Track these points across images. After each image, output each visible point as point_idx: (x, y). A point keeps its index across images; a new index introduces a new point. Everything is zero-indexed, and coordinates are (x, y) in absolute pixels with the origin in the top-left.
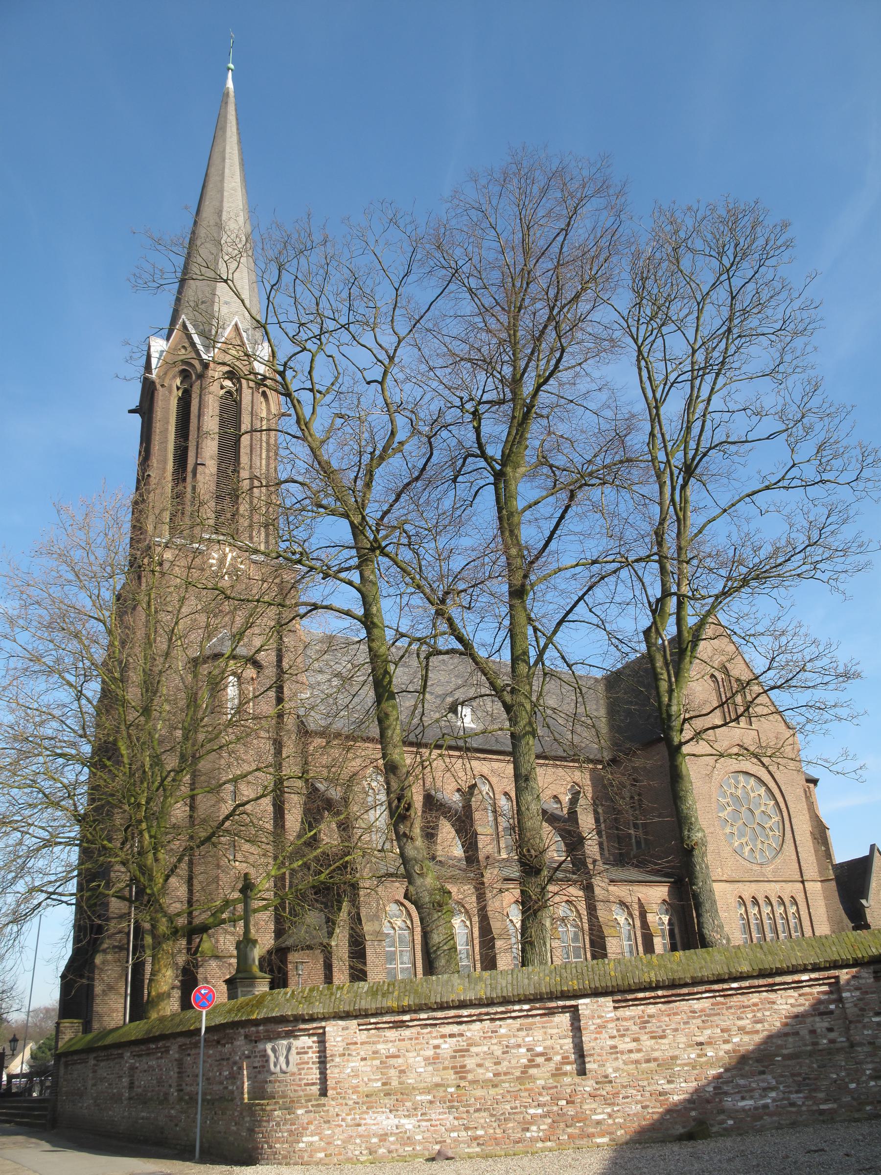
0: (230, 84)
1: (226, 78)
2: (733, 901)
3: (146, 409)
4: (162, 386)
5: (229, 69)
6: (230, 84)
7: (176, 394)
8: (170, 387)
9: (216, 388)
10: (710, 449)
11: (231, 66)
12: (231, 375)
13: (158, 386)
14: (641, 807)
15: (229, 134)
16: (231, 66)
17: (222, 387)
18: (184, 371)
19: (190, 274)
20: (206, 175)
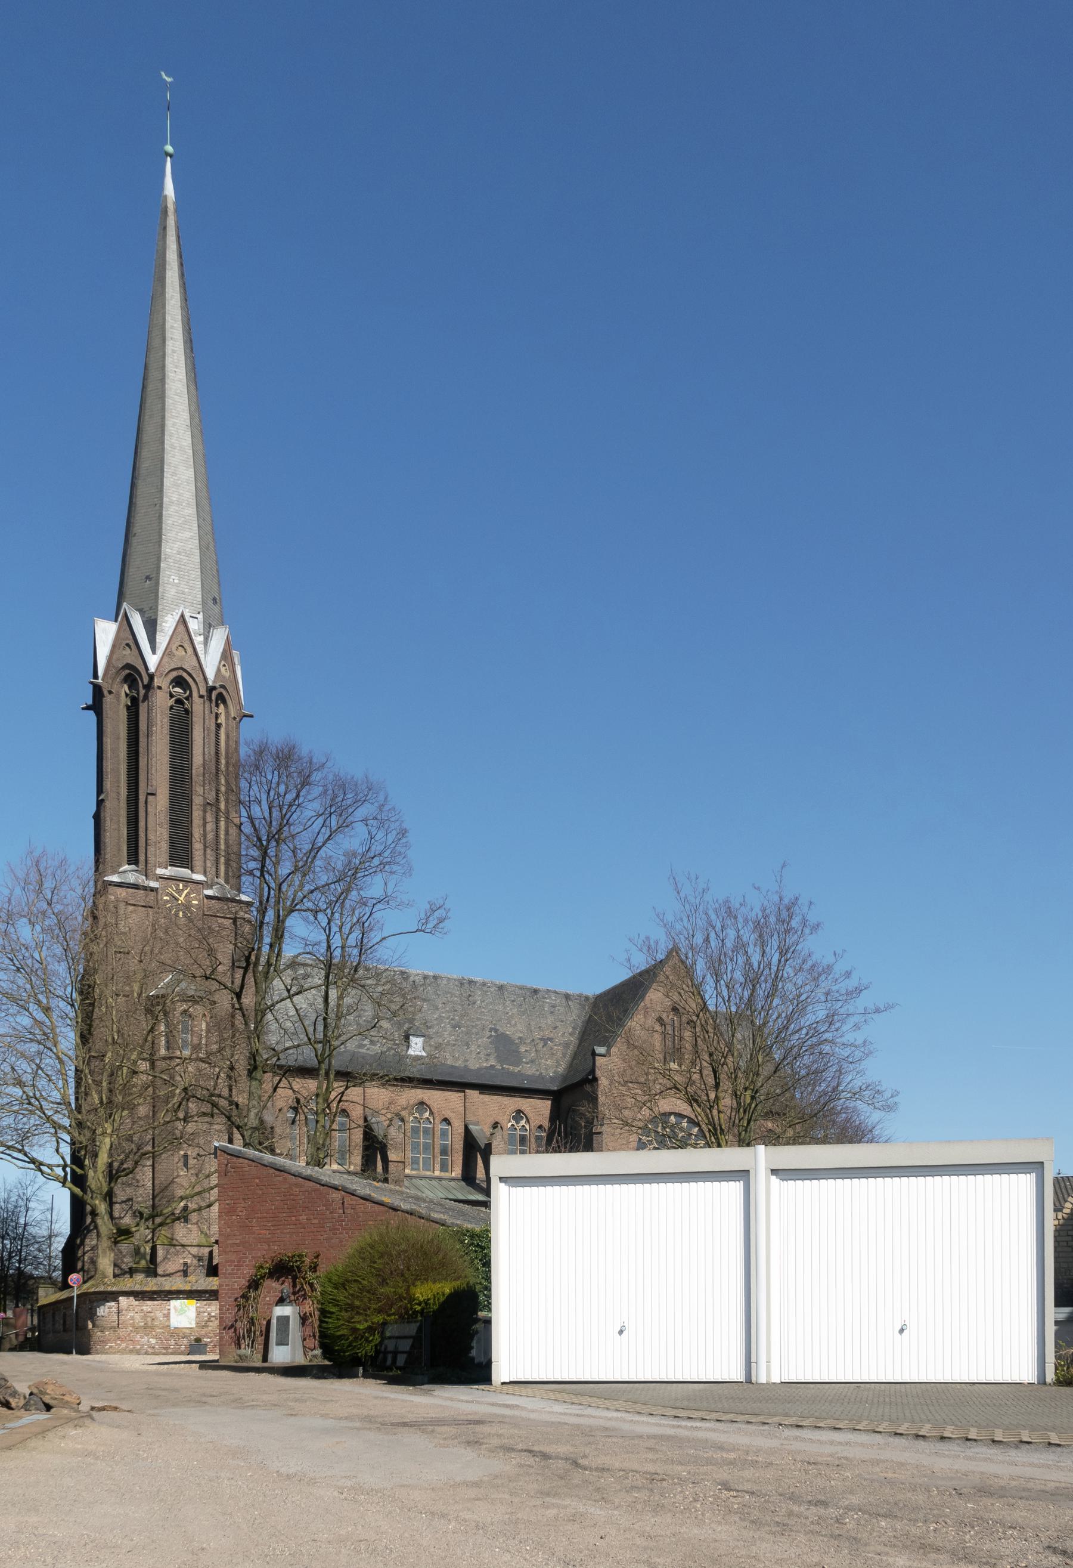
0: (169, 189)
1: (165, 162)
2: (235, 1141)
3: (97, 706)
4: (110, 692)
5: (167, 154)
6: (169, 189)
7: (125, 701)
8: (118, 694)
9: (161, 702)
10: (291, 1088)
11: (169, 148)
12: (179, 682)
13: (106, 693)
14: (212, 1105)
15: (170, 346)
16: (169, 148)
17: (171, 696)
18: (129, 675)
19: (133, 586)
20: (145, 379)
